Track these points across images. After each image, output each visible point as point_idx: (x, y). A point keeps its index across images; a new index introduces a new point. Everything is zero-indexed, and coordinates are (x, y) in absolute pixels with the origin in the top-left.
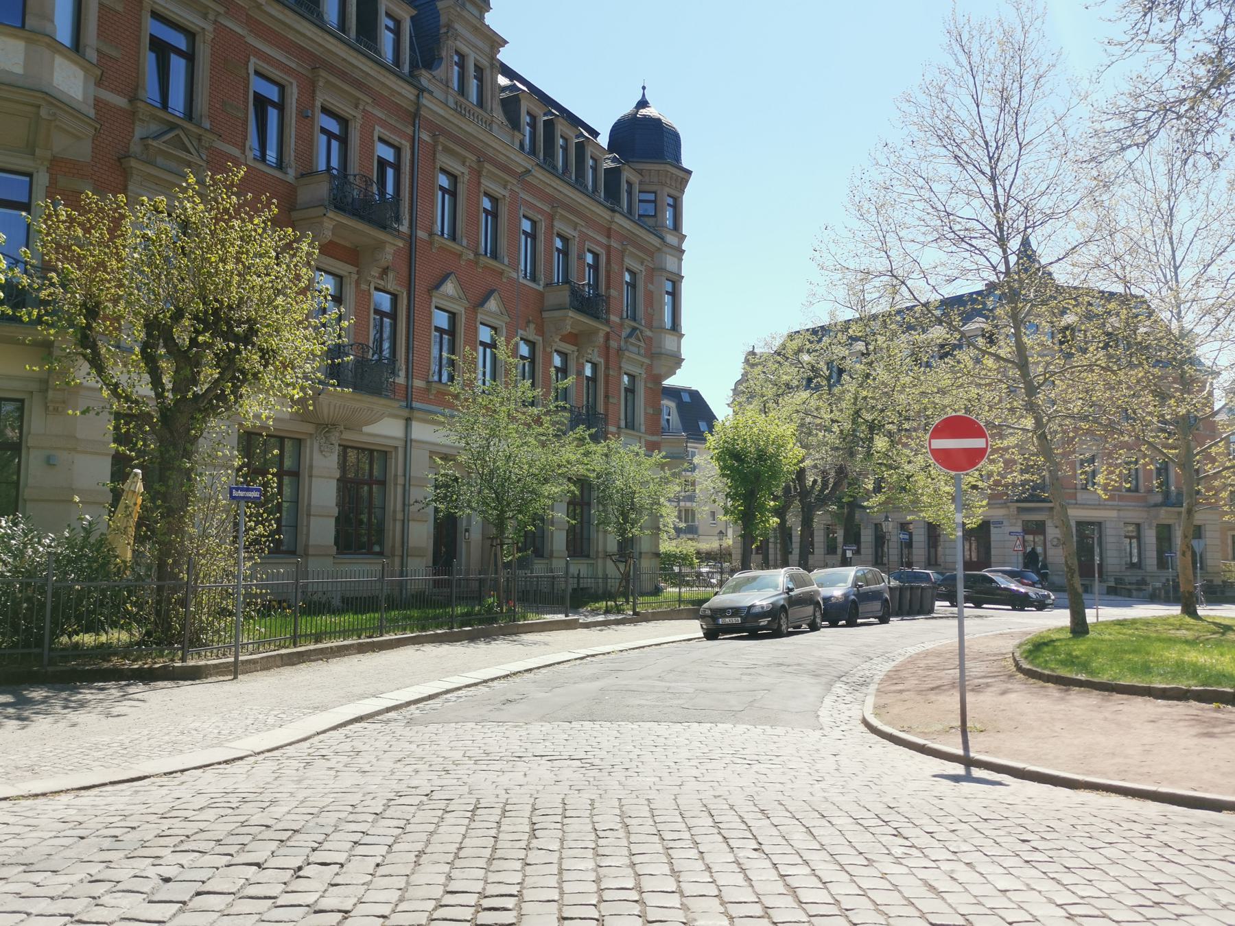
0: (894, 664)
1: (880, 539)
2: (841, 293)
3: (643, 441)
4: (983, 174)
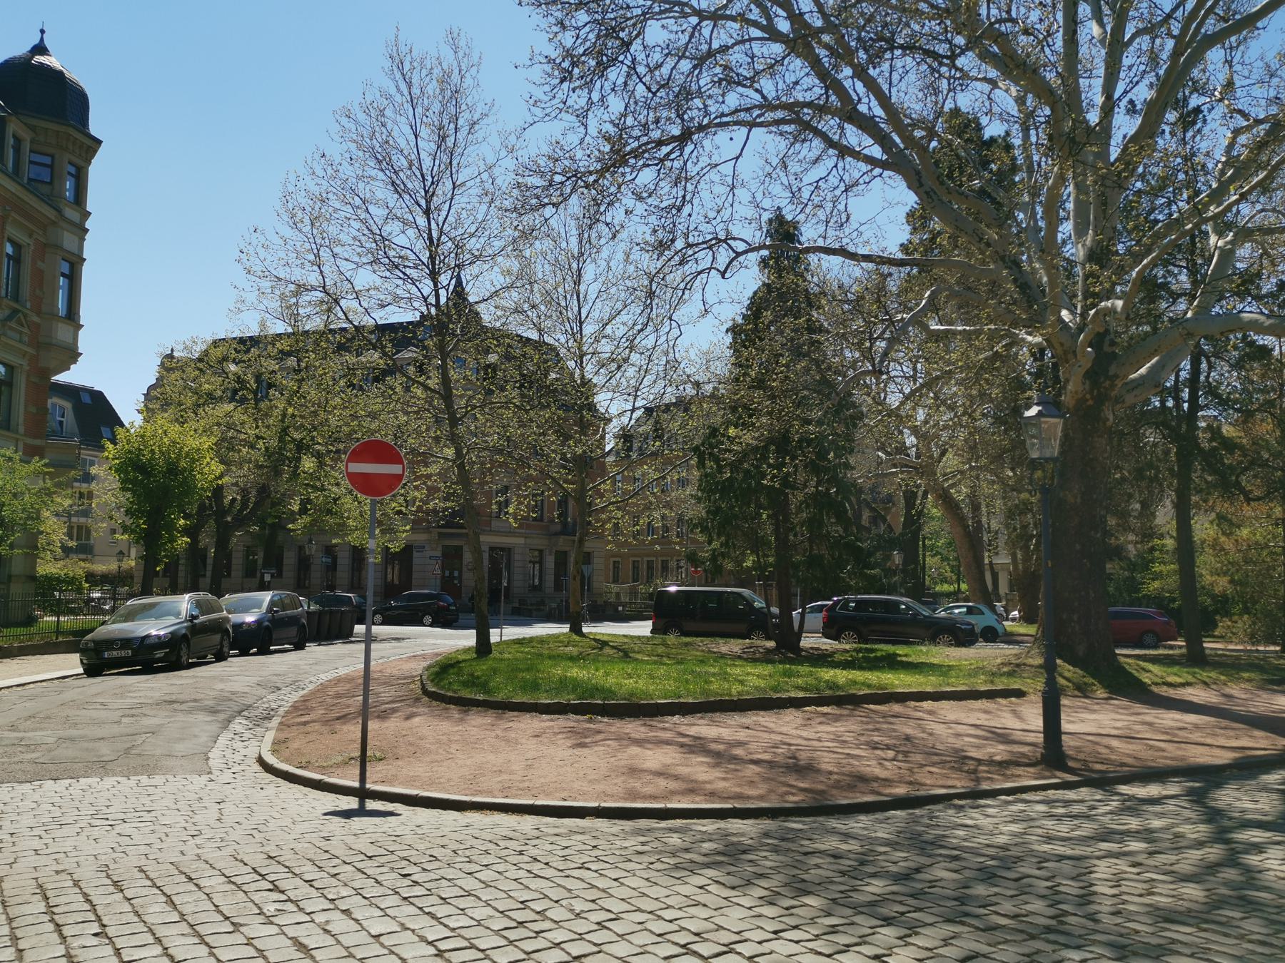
0: (302, 693)
1: (304, 564)
2: (275, 304)
3: (21, 446)
4: (419, 206)
